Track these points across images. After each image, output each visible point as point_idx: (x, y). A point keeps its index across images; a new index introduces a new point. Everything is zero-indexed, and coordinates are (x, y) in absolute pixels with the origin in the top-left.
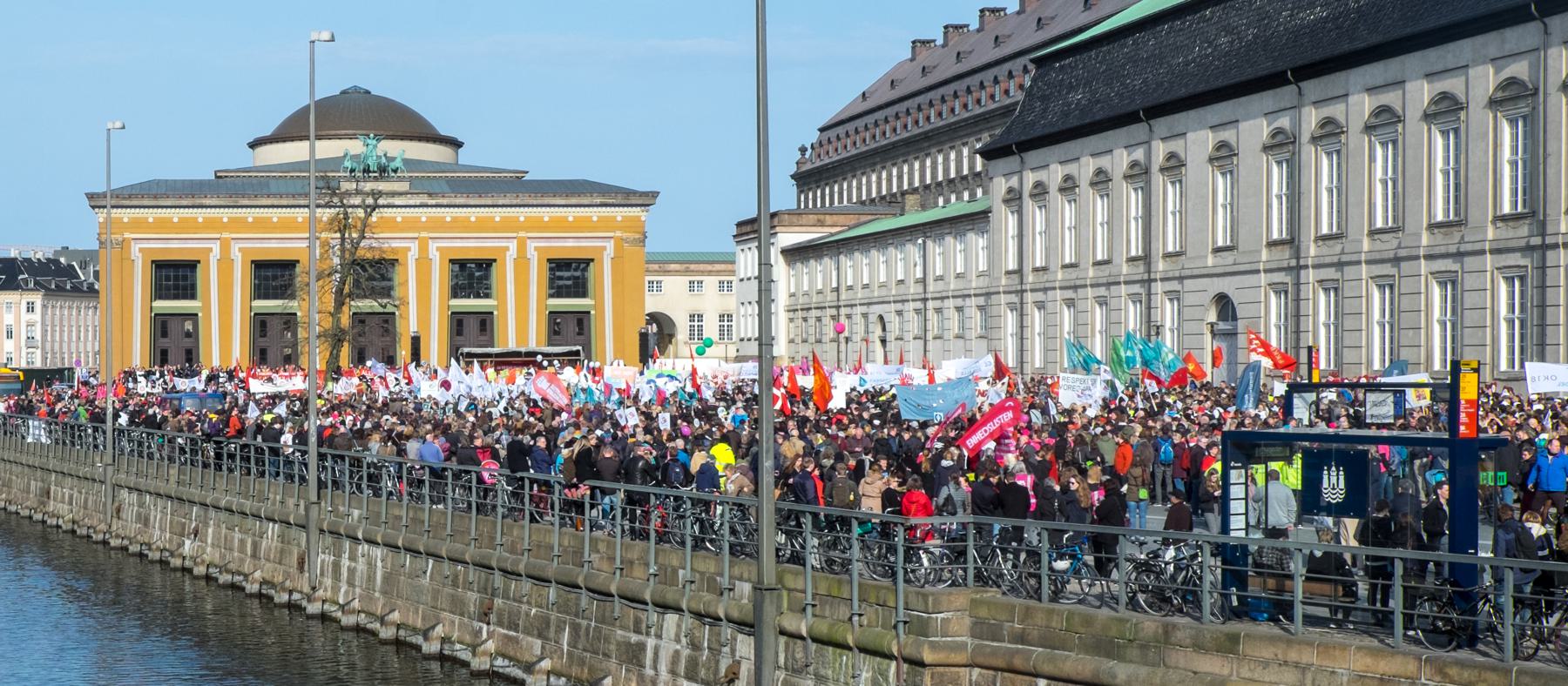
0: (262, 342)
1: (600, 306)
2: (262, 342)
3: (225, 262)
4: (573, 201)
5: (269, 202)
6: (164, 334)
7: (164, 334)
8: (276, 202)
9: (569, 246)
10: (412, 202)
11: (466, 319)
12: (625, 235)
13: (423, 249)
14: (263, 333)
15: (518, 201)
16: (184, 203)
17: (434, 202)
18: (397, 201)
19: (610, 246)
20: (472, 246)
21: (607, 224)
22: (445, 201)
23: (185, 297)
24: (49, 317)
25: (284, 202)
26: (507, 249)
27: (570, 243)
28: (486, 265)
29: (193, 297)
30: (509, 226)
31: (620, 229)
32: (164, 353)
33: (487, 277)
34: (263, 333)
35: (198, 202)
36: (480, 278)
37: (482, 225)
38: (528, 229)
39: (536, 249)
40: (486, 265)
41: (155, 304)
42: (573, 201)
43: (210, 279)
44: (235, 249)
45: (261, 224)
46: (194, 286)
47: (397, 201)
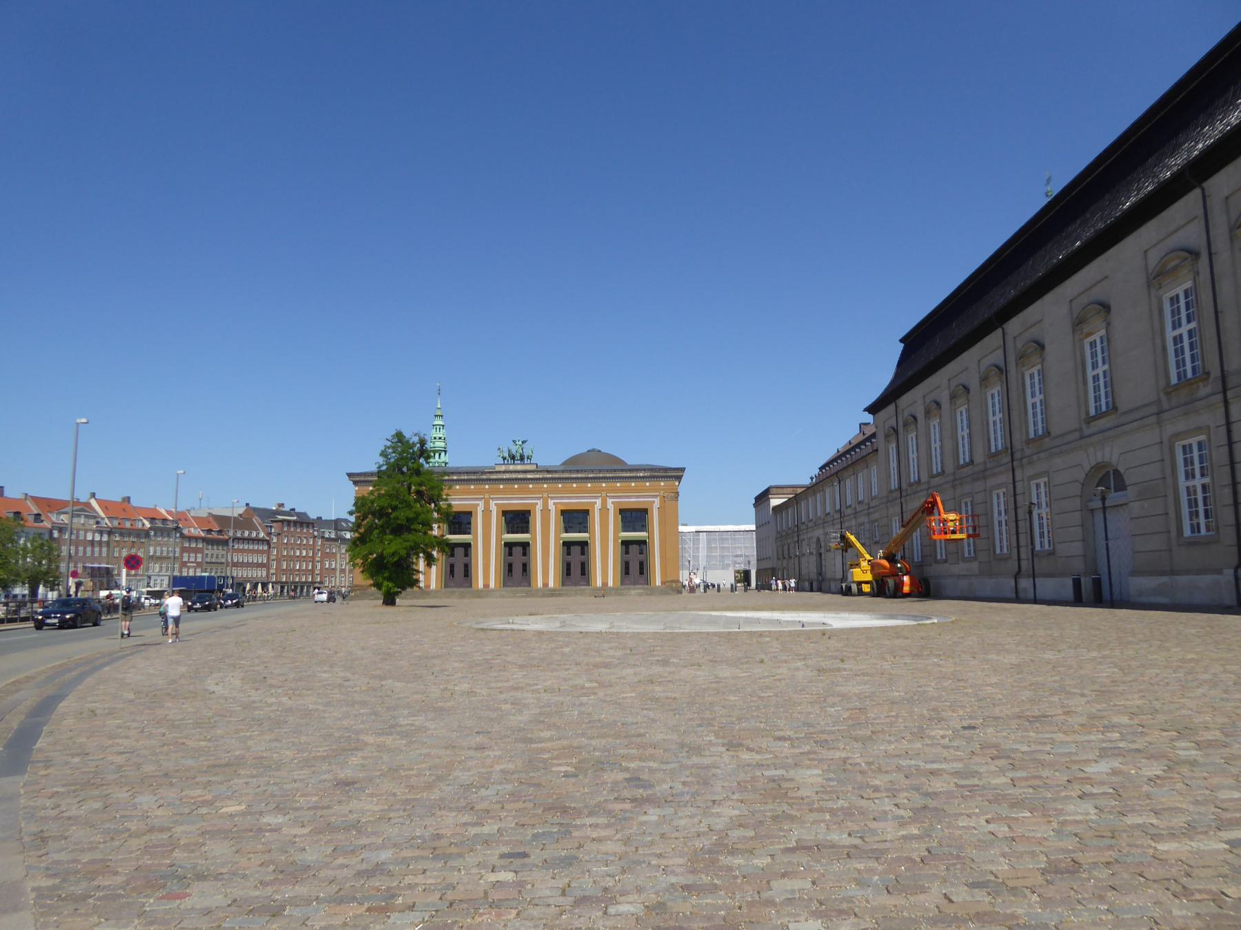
18: (529, 476)
19: (657, 501)
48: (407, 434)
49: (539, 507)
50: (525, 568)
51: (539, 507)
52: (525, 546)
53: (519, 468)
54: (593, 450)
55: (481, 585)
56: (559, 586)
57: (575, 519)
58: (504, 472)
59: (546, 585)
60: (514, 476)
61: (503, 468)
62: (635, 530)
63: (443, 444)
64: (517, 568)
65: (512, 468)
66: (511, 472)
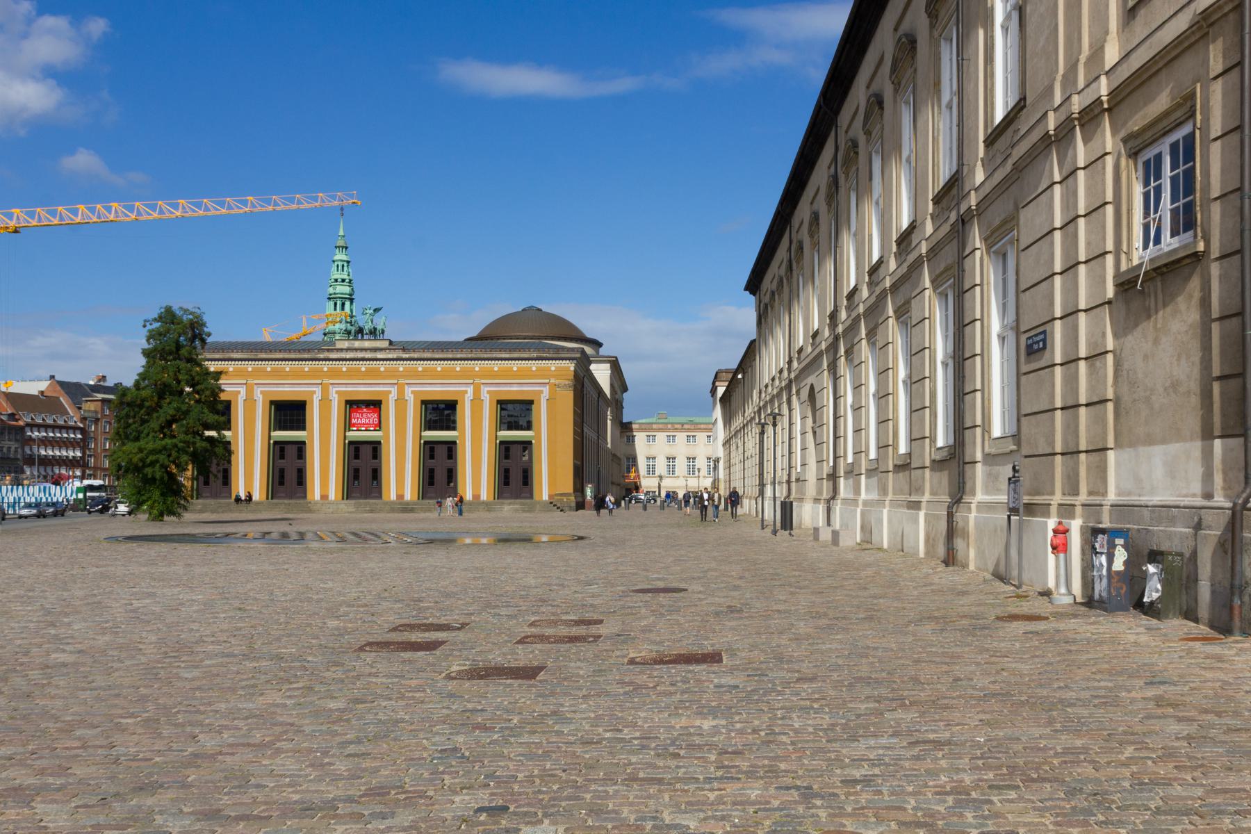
0: (281, 463)
1: (311, 436)
2: (449, 463)
3: (401, 401)
4: (516, 355)
5: (281, 356)
6: (432, 457)
7: (507, 457)
8: (287, 356)
9: (514, 390)
10: (390, 356)
11: (288, 448)
12: (557, 382)
13: (401, 392)
14: (357, 457)
15: (473, 355)
16: (217, 356)
17: (407, 356)
18: (379, 355)
19: (546, 391)
20: (439, 390)
21: (542, 373)
22: (416, 355)
23: (448, 428)
24: (768, 443)
25: (293, 356)
26: (466, 392)
27: (515, 388)
28: (452, 405)
29: (454, 429)
30: (465, 374)
31: (553, 376)
32: (357, 471)
33: (530, 410)
34: (357, 457)
35: (227, 356)
36: (449, 415)
37: (445, 375)
38: (330, 377)
39: (262, 392)
40: (452, 405)
41: (273, 434)
42: (516, 355)
43: (465, 415)
44: (333, 391)
45: (276, 373)
46: (454, 422)
47: (379, 355)
48: (175, 308)
49: (393, 396)
50: (376, 474)
51: (393, 396)
52: (300, 447)
53: (367, 344)
54: (531, 308)
55: (317, 497)
56: (410, 494)
57: (515, 413)
58: (348, 350)
59: (400, 497)
60: (360, 355)
61: (346, 344)
62: (292, 429)
63: (347, 290)
64: (366, 474)
65: (357, 344)
66: (356, 350)
